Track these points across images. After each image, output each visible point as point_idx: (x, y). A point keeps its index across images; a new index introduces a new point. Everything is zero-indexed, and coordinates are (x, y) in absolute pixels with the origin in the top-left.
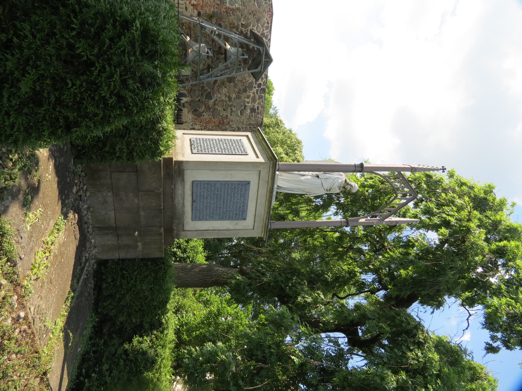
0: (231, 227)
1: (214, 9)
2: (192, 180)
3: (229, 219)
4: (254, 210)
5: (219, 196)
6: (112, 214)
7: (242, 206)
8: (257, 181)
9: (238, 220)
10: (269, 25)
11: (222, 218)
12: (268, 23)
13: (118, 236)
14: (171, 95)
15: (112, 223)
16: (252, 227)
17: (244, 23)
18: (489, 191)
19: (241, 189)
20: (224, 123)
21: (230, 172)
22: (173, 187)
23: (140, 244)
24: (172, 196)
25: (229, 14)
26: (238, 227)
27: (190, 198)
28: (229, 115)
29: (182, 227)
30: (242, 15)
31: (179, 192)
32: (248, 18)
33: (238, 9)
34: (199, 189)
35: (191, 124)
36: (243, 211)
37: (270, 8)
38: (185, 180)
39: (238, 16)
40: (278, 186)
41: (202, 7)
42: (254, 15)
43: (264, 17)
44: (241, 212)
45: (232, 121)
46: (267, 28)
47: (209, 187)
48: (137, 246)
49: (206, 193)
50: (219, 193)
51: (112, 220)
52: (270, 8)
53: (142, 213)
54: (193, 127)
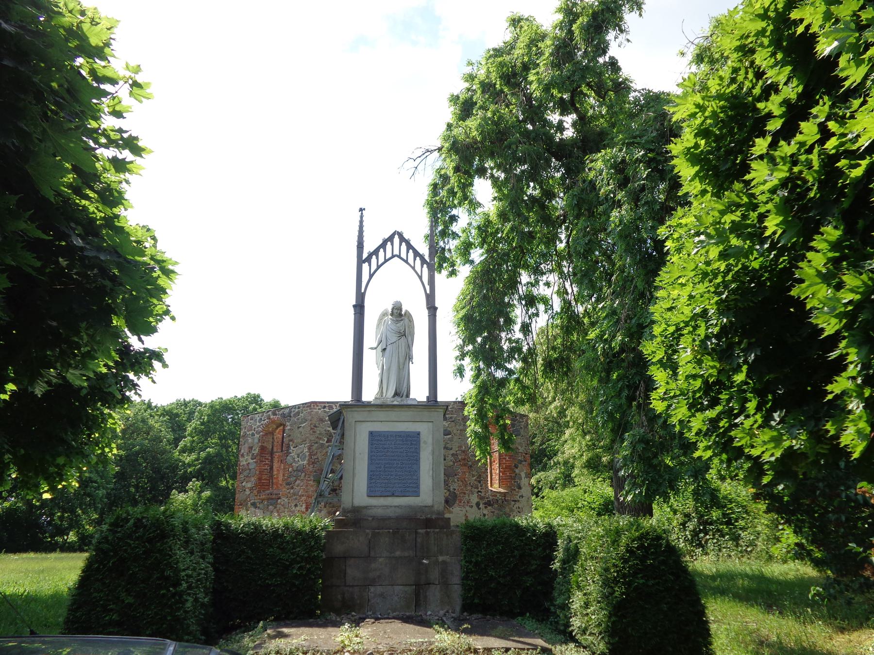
0: (430, 448)
2: (366, 497)
3: (419, 453)
6: (398, 588)
9: (419, 441)
12: (325, 407)
14: (746, 583)
15: (410, 589)
16: (430, 424)
18: (454, 99)
20: (464, 459)
21: (357, 455)
23: (441, 559)
24: (382, 521)
26: (430, 441)
27: (390, 499)
28: (451, 452)
31: (379, 512)
32: (320, 434)
33: (309, 449)
35: (468, 508)
36: (408, 436)
39: (317, 449)
40: (396, 394)
41: (308, 497)
43: (317, 413)
45: (461, 447)
46: (331, 408)
48: (444, 562)
51: (407, 588)
53: (398, 553)
54: (474, 505)
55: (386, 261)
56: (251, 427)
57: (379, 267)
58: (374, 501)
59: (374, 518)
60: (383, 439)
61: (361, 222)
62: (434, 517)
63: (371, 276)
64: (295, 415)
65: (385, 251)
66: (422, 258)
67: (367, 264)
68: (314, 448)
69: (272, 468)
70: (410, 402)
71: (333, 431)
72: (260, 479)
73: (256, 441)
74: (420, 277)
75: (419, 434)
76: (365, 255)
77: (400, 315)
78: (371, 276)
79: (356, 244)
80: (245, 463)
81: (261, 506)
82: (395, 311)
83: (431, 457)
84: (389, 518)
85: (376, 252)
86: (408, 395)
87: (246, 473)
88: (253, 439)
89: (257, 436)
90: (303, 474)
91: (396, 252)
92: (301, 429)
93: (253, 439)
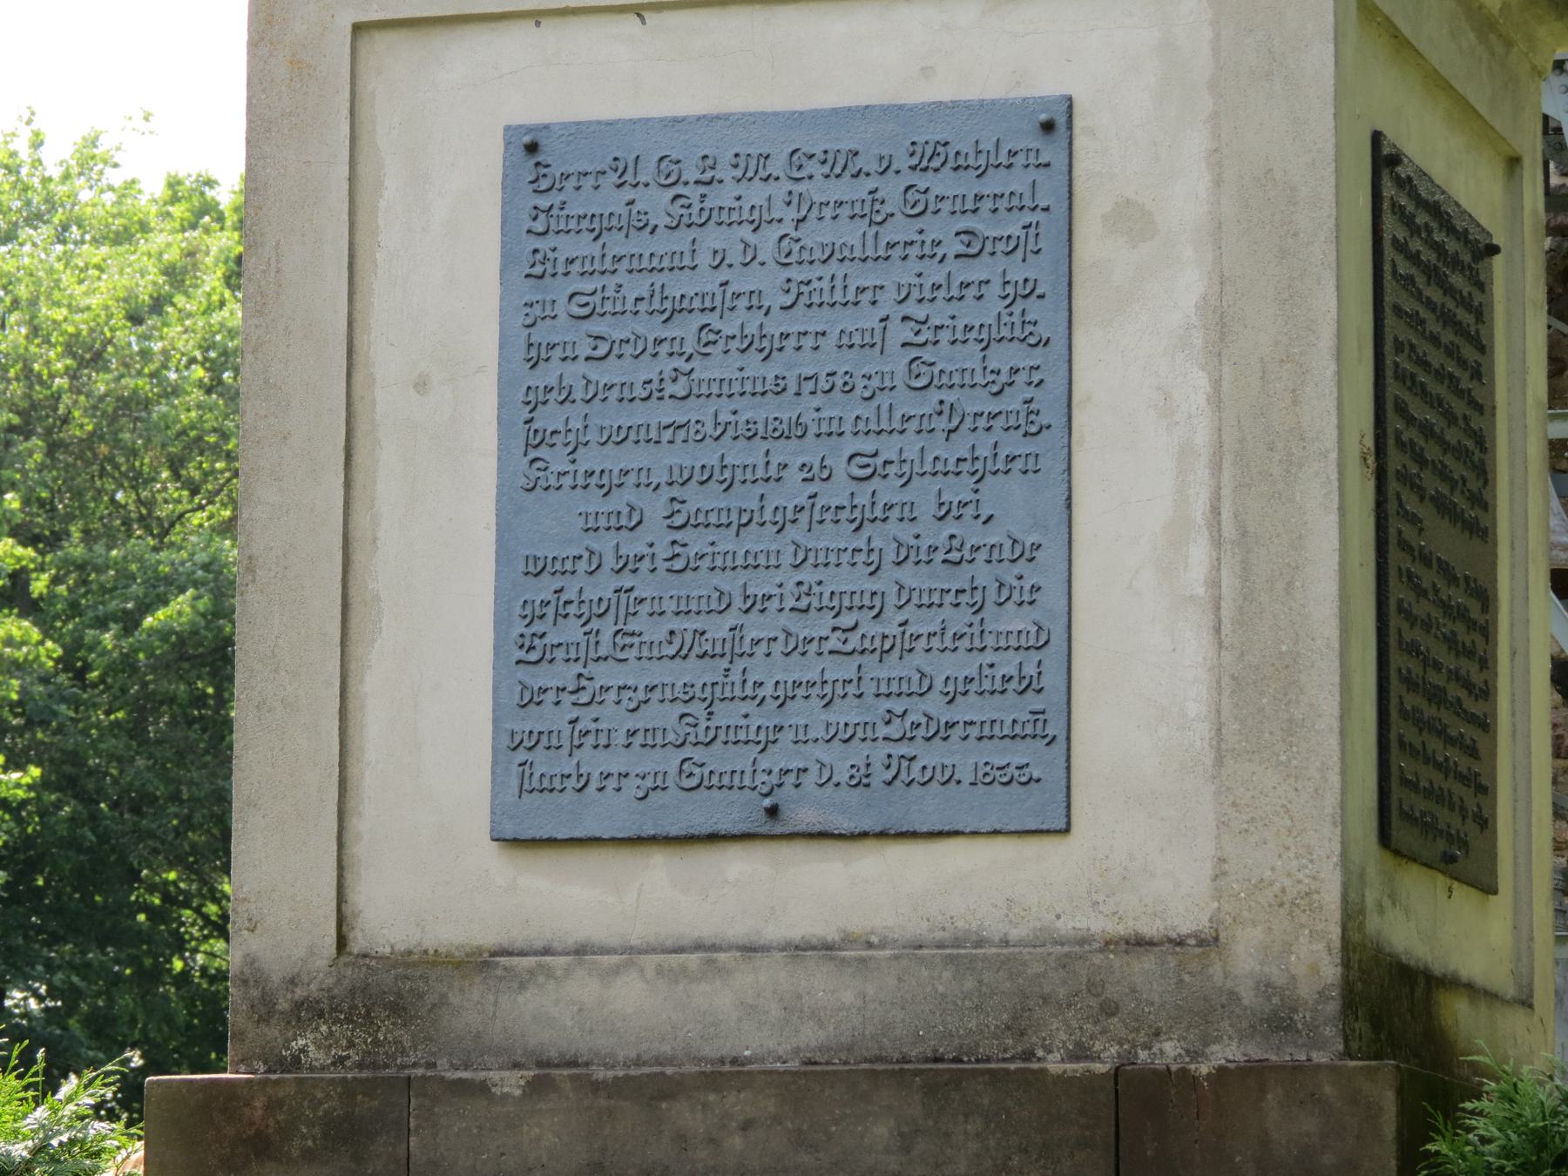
0: (1187, 288)
5: (698, 499)
7: (843, 189)
8: (514, 43)
11: (1031, 427)
19: (599, 228)
21: (387, 396)
22: (510, 1083)
26: (1186, 198)
27: (738, 866)
29: (1147, 963)
31: (629, 1014)
34: (594, 762)
38: (487, 937)
44: (943, 184)
49: (660, 673)
50: (655, 508)
59: (551, 1074)
60: (656, 203)
62: (1226, 1052)
75: (1055, 124)
83: (1194, 386)
84: (728, 1075)
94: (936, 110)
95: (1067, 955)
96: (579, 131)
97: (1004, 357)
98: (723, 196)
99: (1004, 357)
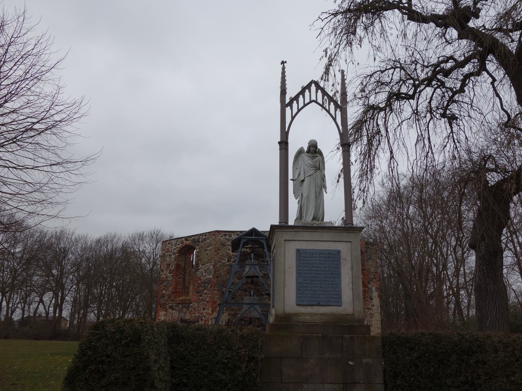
0: (349, 265)
1: (215, 290)
3: (339, 268)
4: (328, 243)
8: (296, 242)
9: (340, 259)
10: (227, 234)
11: (338, 275)
12: (225, 235)
13: (356, 383)
16: (349, 244)
17: (227, 260)
22: (300, 324)
23: (364, 361)
25: (219, 275)
26: (349, 258)
27: (316, 307)
30: (220, 262)
32: (222, 255)
33: (214, 266)
37: (212, 235)
40: (314, 219)
42: (219, 249)
43: (220, 239)
47: (303, 288)
52: (212, 235)
55: (305, 105)
56: (169, 249)
57: (299, 110)
58: (302, 310)
61: (283, 73)
63: (293, 118)
64: (203, 241)
65: (304, 97)
66: (335, 103)
67: (289, 107)
68: (218, 266)
69: (184, 280)
70: (323, 225)
71: (232, 253)
72: (176, 288)
73: (173, 260)
74: (335, 119)
75: (339, 252)
76: (287, 101)
77: (315, 152)
78: (293, 118)
79: (280, 90)
80: (164, 276)
81: (177, 308)
82: (312, 149)
83: (350, 272)
85: (296, 98)
86: (323, 220)
87: (165, 284)
88: (170, 258)
89: (173, 256)
90: (210, 285)
91: (313, 98)
92: (207, 252)
93: (170, 258)
94: (330, 250)
95: (269, 278)
96: (302, 250)
97: (336, 269)
98: (314, 255)
99: (336, 269)
